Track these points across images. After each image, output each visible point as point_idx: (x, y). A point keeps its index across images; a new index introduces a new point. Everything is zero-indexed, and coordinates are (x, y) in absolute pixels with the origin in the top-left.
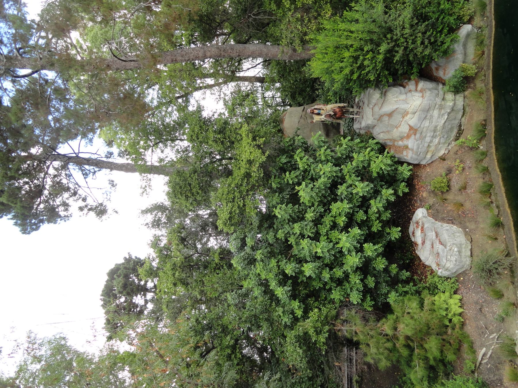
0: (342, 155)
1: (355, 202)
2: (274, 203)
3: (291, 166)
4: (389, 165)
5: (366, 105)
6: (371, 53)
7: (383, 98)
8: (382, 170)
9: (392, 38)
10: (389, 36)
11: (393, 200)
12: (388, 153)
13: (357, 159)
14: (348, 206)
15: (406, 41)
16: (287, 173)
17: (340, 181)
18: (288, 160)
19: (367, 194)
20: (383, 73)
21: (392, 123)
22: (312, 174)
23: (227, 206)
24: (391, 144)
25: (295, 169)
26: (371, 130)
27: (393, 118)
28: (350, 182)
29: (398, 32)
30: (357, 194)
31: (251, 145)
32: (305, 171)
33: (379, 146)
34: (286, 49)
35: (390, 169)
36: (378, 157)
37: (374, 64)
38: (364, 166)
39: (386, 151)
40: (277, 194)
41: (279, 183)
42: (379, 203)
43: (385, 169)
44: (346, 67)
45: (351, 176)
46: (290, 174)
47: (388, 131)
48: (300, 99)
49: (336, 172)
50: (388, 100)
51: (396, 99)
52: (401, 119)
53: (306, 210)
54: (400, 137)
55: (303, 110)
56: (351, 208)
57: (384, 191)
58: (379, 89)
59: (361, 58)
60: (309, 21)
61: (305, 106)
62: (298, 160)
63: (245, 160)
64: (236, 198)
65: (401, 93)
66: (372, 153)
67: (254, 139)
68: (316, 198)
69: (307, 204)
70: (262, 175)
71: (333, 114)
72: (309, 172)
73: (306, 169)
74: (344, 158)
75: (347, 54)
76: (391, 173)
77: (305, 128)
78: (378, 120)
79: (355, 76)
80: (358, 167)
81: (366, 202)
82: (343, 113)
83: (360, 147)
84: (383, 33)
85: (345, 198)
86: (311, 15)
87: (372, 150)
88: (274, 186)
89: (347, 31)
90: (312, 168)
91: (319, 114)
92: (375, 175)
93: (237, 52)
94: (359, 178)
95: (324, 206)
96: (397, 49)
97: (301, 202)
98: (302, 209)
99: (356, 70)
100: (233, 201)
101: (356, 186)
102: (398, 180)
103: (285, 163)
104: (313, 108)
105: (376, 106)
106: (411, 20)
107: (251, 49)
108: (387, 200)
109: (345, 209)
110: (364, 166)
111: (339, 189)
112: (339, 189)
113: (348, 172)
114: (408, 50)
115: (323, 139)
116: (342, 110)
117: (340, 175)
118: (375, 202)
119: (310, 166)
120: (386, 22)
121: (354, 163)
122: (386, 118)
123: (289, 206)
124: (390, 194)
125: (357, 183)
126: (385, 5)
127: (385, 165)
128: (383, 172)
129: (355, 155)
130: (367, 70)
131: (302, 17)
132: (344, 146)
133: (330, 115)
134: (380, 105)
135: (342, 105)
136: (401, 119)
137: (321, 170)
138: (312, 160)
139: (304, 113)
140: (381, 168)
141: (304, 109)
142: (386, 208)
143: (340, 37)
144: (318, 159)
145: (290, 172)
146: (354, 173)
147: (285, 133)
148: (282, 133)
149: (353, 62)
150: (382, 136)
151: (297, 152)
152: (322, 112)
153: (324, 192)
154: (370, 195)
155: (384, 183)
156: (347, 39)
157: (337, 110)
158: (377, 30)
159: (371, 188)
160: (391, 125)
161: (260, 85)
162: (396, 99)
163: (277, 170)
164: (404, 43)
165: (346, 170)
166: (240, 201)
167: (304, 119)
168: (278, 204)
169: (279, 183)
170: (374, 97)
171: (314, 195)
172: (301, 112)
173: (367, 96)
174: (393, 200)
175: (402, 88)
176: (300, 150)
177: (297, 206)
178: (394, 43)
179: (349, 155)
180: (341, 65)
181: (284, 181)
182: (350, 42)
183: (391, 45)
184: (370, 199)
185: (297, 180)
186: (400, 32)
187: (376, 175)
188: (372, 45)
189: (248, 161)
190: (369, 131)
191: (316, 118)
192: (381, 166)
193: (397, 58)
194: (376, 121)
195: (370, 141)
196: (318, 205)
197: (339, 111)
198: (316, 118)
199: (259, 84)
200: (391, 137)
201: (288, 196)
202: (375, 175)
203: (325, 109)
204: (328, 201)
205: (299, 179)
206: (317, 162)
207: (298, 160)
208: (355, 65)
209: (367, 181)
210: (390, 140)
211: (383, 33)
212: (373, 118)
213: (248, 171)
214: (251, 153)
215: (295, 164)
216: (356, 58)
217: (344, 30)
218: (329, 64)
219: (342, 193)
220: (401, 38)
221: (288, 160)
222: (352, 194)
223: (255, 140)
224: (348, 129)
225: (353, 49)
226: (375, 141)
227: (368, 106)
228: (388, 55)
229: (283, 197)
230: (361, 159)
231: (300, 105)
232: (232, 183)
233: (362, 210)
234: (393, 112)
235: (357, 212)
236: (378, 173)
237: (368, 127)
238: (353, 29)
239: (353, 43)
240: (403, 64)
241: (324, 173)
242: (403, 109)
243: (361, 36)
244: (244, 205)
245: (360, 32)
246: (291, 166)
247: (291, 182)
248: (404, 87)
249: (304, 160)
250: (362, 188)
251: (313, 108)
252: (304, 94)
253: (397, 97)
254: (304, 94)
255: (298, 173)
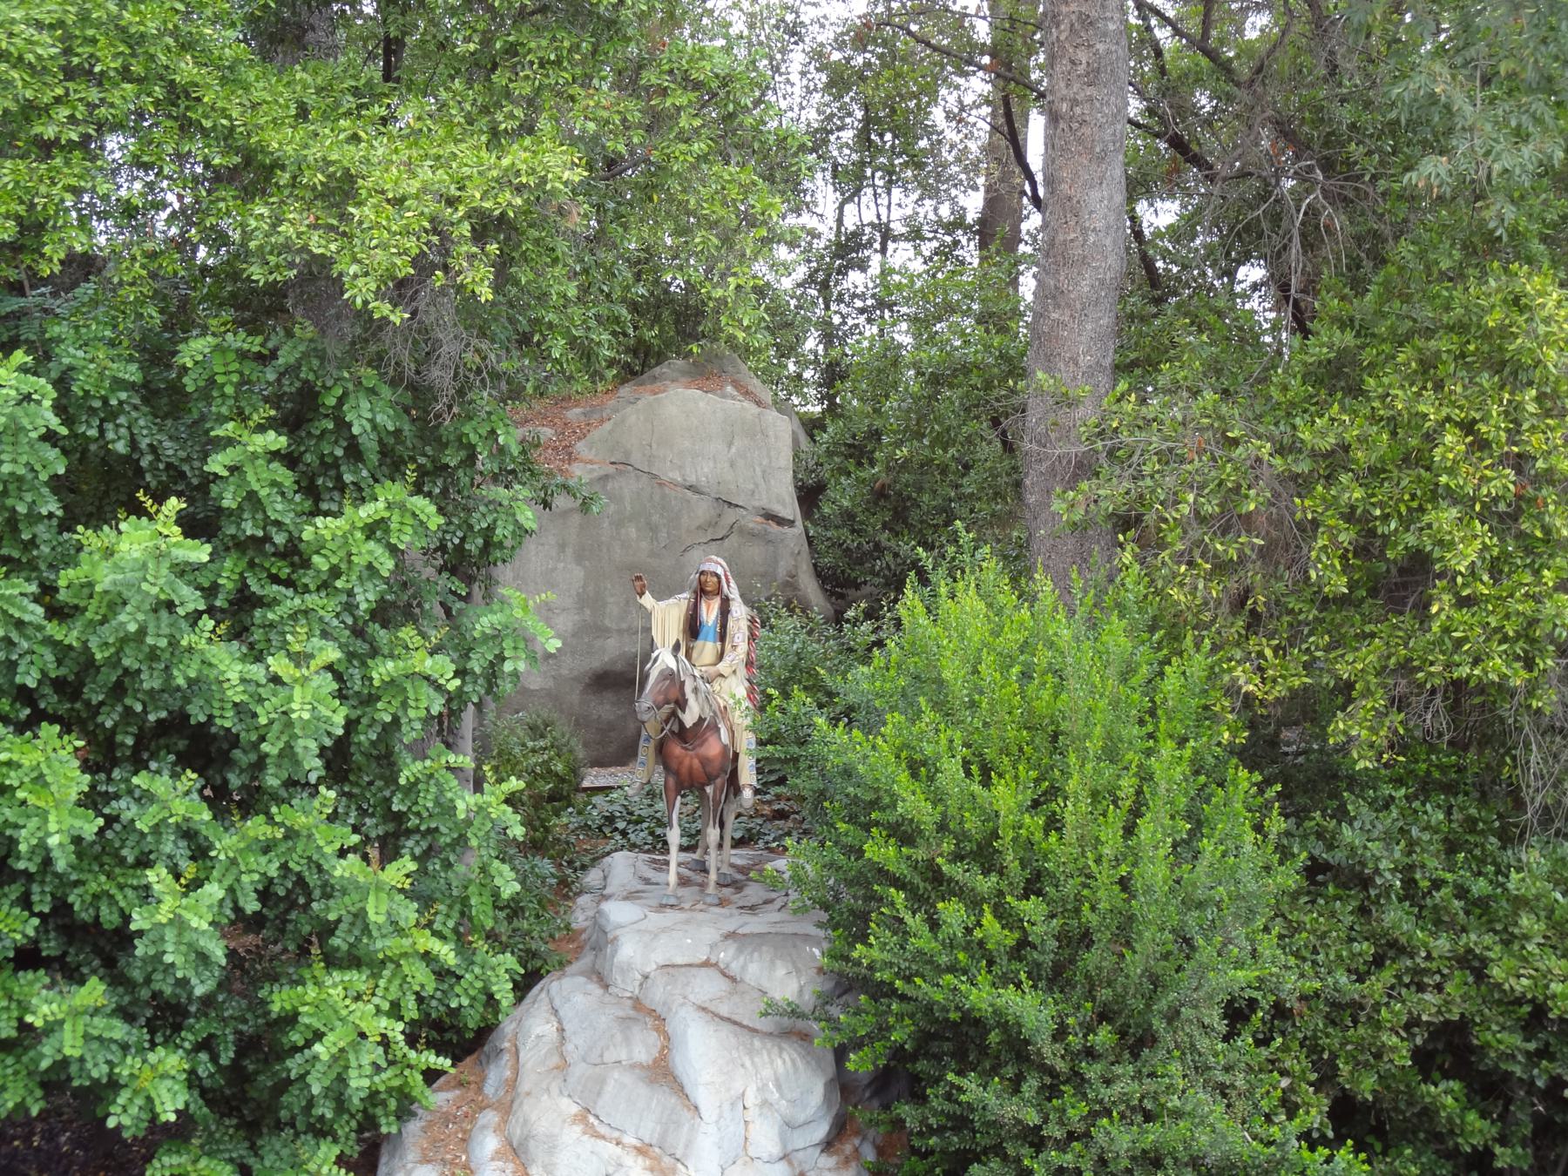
0: (412, 788)
1: (93, 887)
2: (70, 354)
3: (330, 465)
4: (341, 1080)
5: (734, 921)
6: (1011, 939)
7: (765, 1024)
8: (308, 1044)
9: (1090, 1053)
10: (1104, 1036)
11: (111, 1123)
12: (431, 1076)
13: (379, 887)
14: (53, 841)
15: (1071, 1136)
16: (275, 440)
17: (234, 780)
18: (370, 444)
19: (145, 960)
20: (900, 1017)
21: (610, 1087)
22: (272, 603)
23: (39, 25)
24: (489, 1089)
25: (309, 489)
26: (586, 960)
27: (643, 1090)
28: (225, 845)
29: (1126, 1085)
30: (146, 894)
31: (451, 202)
32: (295, 553)
33: (472, 1020)
34: (1086, 415)
35: (316, 1090)
36: (395, 1011)
37: (944, 960)
38: (329, 929)
39: (444, 1063)
40: (132, 373)
41: (211, 381)
42: (87, 1037)
43: (316, 1058)
44: (937, 799)
45: (267, 848)
46: (275, 455)
47: (563, 1066)
48: (842, 496)
49: (288, 753)
50: (751, 1052)
51: (751, 1099)
52: (629, 1140)
53: (32, 566)
54: (526, 1138)
55: (770, 517)
56: (47, 862)
57: (172, 1061)
58: (825, 999)
59: (985, 884)
60: (1222, 567)
61: (799, 526)
62: (367, 512)
63: (354, 153)
64: (94, 95)
65: (790, 1125)
66: (421, 976)
67: (485, 227)
68: (108, 633)
69: (65, 577)
70: (257, 273)
71: (689, 719)
72: (289, 583)
73: (306, 564)
74: (388, 801)
75: (1005, 797)
76: (292, 1101)
77: (653, 529)
78: (637, 1003)
79: (881, 851)
80: (327, 896)
81: (98, 951)
82: (687, 783)
83: (465, 901)
84: (1120, 999)
85: (111, 820)
86: (1254, 575)
87: (443, 974)
88: (194, 349)
89: (1139, 792)
90: (312, 600)
91: (693, 628)
92: (280, 1000)
93: (1075, 102)
94: (251, 905)
95: (59, 685)
96: (1031, 1085)
97: (83, 533)
98: (32, 543)
99: (920, 854)
100: (70, 73)
101: (196, 884)
102: (254, 1149)
103: (343, 425)
104: (734, 593)
105: (722, 985)
106: (1183, 1156)
107: (1095, 195)
108: (114, 1085)
109: (33, 823)
110: (329, 929)
111: (175, 776)
112: (175, 776)
113: (291, 834)
114: (1026, 1151)
115: (508, 667)
116: (710, 779)
117: (272, 780)
118: (96, 1011)
119: (325, 586)
120: (1173, 1016)
121: (346, 869)
122: (643, 1048)
123: (52, 454)
124: (149, 1099)
125: (214, 891)
126: (1292, 1003)
127: (340, 1056)
128: (296, 1049)
129: (400, 871)
130: (914, 922)
131: (1247, 520)
132: (465, 802)
133: (681, 704)
134: (724, 1010)
135: (748, 775)
136: (629, 1140)
137: (299, 659)
138: (366, 598)
139: (754, 522)
140: (319, 1036)
141: (781, 521)
142: (54, 1082)
143: (1111, 753)
144: (382, 636)
145: (289, 459)
146: (284, 867)
147: (626, 391)
148: (629, 374)
149: (961, 837)
150: (538, 1030)
151: (424, 506)
152: (707, 648)
153: (150, 681)
154: (137, 975)
155: (227, 1056)
156: (1095, 795)
157: (712, 749)
158: (1135, 965)
159: (183, 983)
160: (601, 1082)
161: (971, 217)
162: (751, 1099)
163: (291, 370)
164: (1061, 1123)
165: (300, 820)
166: (72, 119)
167: (713, 524)
168: (62, 383)
169: (211, 381)
170: (781, 971)
171: (129, 621)
172: (763, 501)
173: (789, 929)
174: (111, 1123)
175: (821, 1130)
176: (435, 521)
177: (52, 506)
178: (1061, 1066)
179: (409, 833)
180: (951, 768)
181: (223, 419)
182: (1073, 812)
183: (1050, 1053)
184: (117, 979)
185: (229, 502)
186: (1125, 1098)
187: (275, 1008)
188: (1053, 944)
189: (349, 178)
190: (581, 948)
191: (667, 616)
192: (330, 1038)
193: (971, 1088)
194: (630, 986)
195: (509, 960)
196: (62, 651)
197: (705, 761)
198: (667, 616)
199: (973, 204)
200: (525, 1085)
201: (121, 447)
202: (280, 1000)
203: (722, 667)
204: (95, 710)
205: (236, 515)
206: (358, 632)
207: (367, 512)
208: (948, 846)
209: (231, 954)
210: (512, 1084)
211: (1120, 999)
212: (650, 968)
213: (284, 178)
214: (399, 202)
215: (341, 487)
216: (984, 855)
217: (1146, 777)
218: (960, 690)
219: (145, 798)
220: (1083, 1108)
221: (370, 444)
222: (144, 862)
223: (479, 236)
224: (610, 819)
225: (1038, 836)
226: (503, 991)
227: (731, 936)
228: (994, 1037)
229: (111, 414)
230: (376, 913)
231: (809, 495)
232: (205, 59)
233: (43, 929)
234: (679, 1089)
235: (25, 902)
236: (291, 1019)
237: (600, 941)
238: (1146, 829)
239: (1070, 834)
240: (956, 1129)
241: (276, 680)
242: (688, 1144)
243: (1105, 876)
244: (46, 148)
245: (1123, 870)
246: (330, 465)
247: (217, 464)
248: (828, 1145)
249: (372, 552)
250: (178, 923)
251: (734, 593)
252: (876, 521)
253: (765, 1104)
254: (876, 521)
255: (277, 508)
